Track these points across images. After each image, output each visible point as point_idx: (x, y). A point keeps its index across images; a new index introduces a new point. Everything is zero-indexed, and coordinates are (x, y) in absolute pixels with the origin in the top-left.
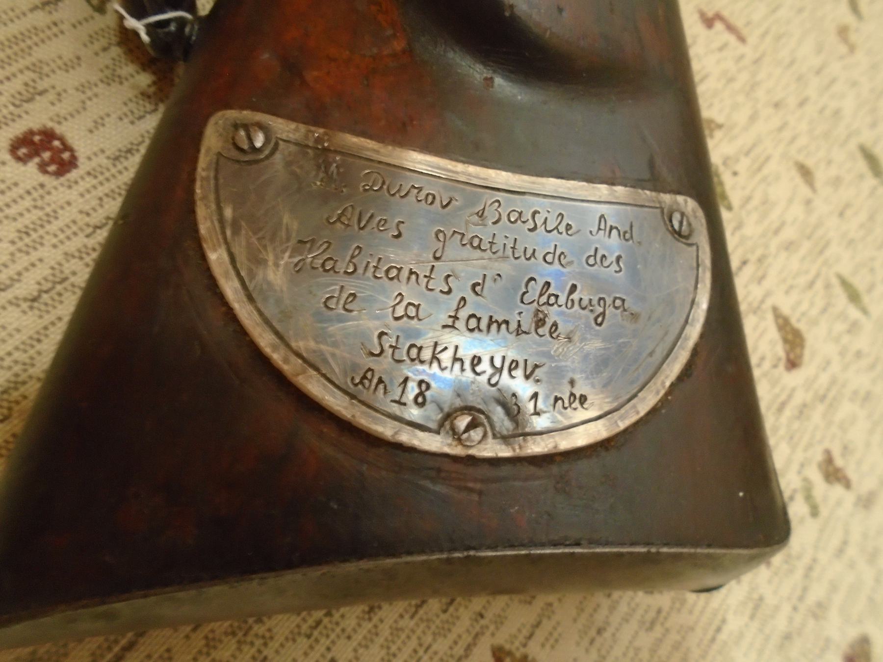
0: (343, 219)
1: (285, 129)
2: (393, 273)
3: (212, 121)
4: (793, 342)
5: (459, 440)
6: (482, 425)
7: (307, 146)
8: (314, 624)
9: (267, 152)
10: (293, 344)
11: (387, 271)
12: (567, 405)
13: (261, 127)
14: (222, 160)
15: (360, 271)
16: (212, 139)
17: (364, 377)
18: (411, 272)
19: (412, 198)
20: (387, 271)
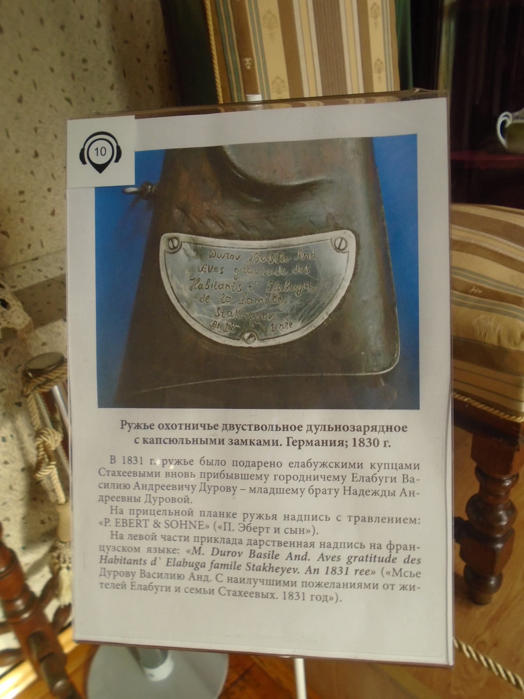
0: (204, 270)
1: (183, 237)
2: (221, 286)
3: (163, 237)
4: (148, 22)
5: (246, 342)
6: (254, 336)
7: (191, 243)
8: (188, 253)
9: (179, 247)
10: (192, 315)
11: (219, 286)
12: (284, 326)
13: (176, 238)
14: (166, 254)
15: (210, 287)
16: (163, 246)
17: (214, 324)
18: (227, 286)
19: (226, 258)
20: (219, 286)
